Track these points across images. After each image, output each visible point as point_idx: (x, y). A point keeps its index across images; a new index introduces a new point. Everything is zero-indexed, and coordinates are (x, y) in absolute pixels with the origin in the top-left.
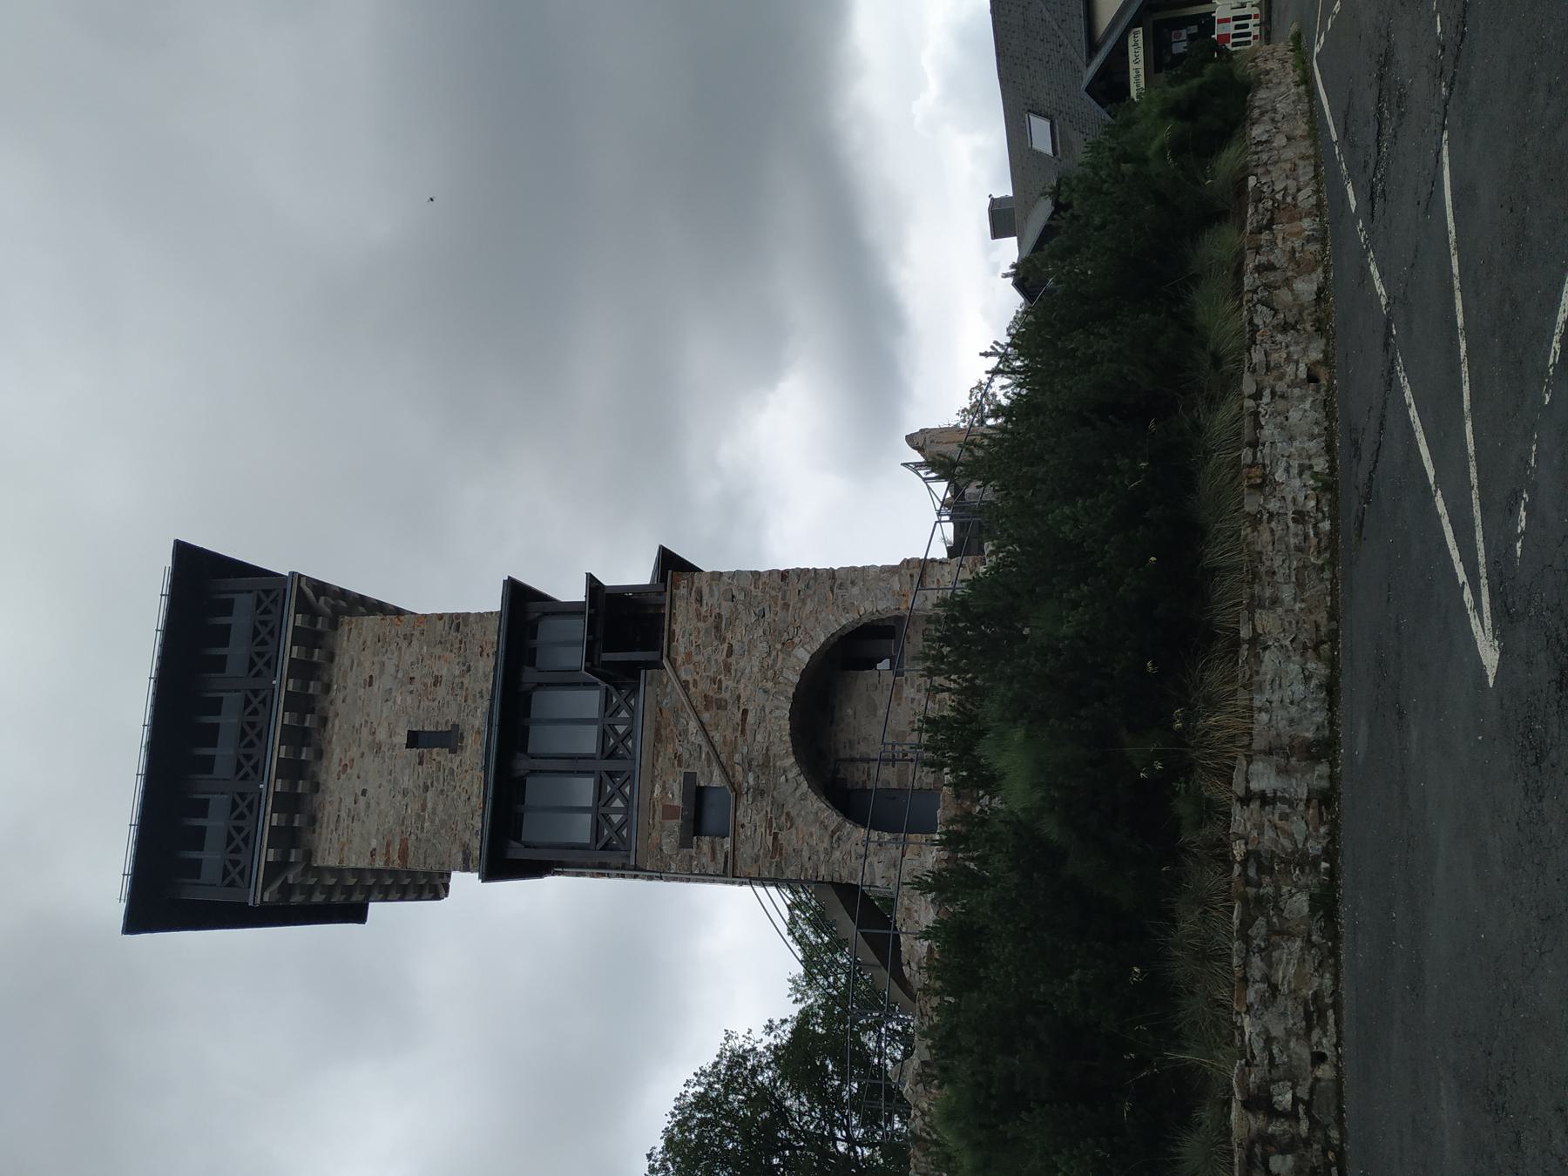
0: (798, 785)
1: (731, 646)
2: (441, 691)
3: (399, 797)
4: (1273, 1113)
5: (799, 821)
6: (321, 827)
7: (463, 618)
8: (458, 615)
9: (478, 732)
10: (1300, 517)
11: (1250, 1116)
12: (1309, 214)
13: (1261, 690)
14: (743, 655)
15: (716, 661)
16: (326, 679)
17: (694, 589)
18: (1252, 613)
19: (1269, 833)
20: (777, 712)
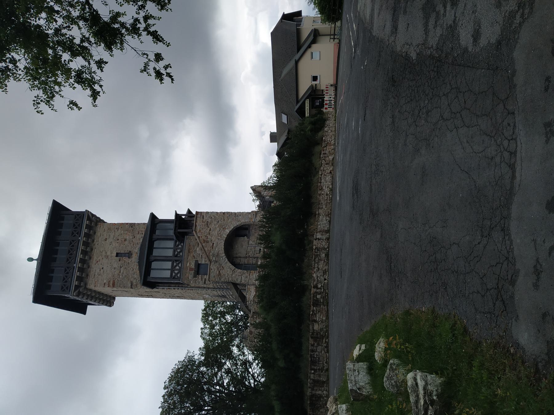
1: (210, 229)
2: (126, 242)
3: (113, 269)
4: (317, 288)
5: (225, 268)
6: (89, 277)
8: (132, 224)
9: (137, 253)
10: (327, 195)
11: (314, 289)
12: (333, 145)
13: (319, 222)
14: (213, 231)
15: (207, 232)
16: (93, 238)
18: (319, 210)
19: (319, 244)
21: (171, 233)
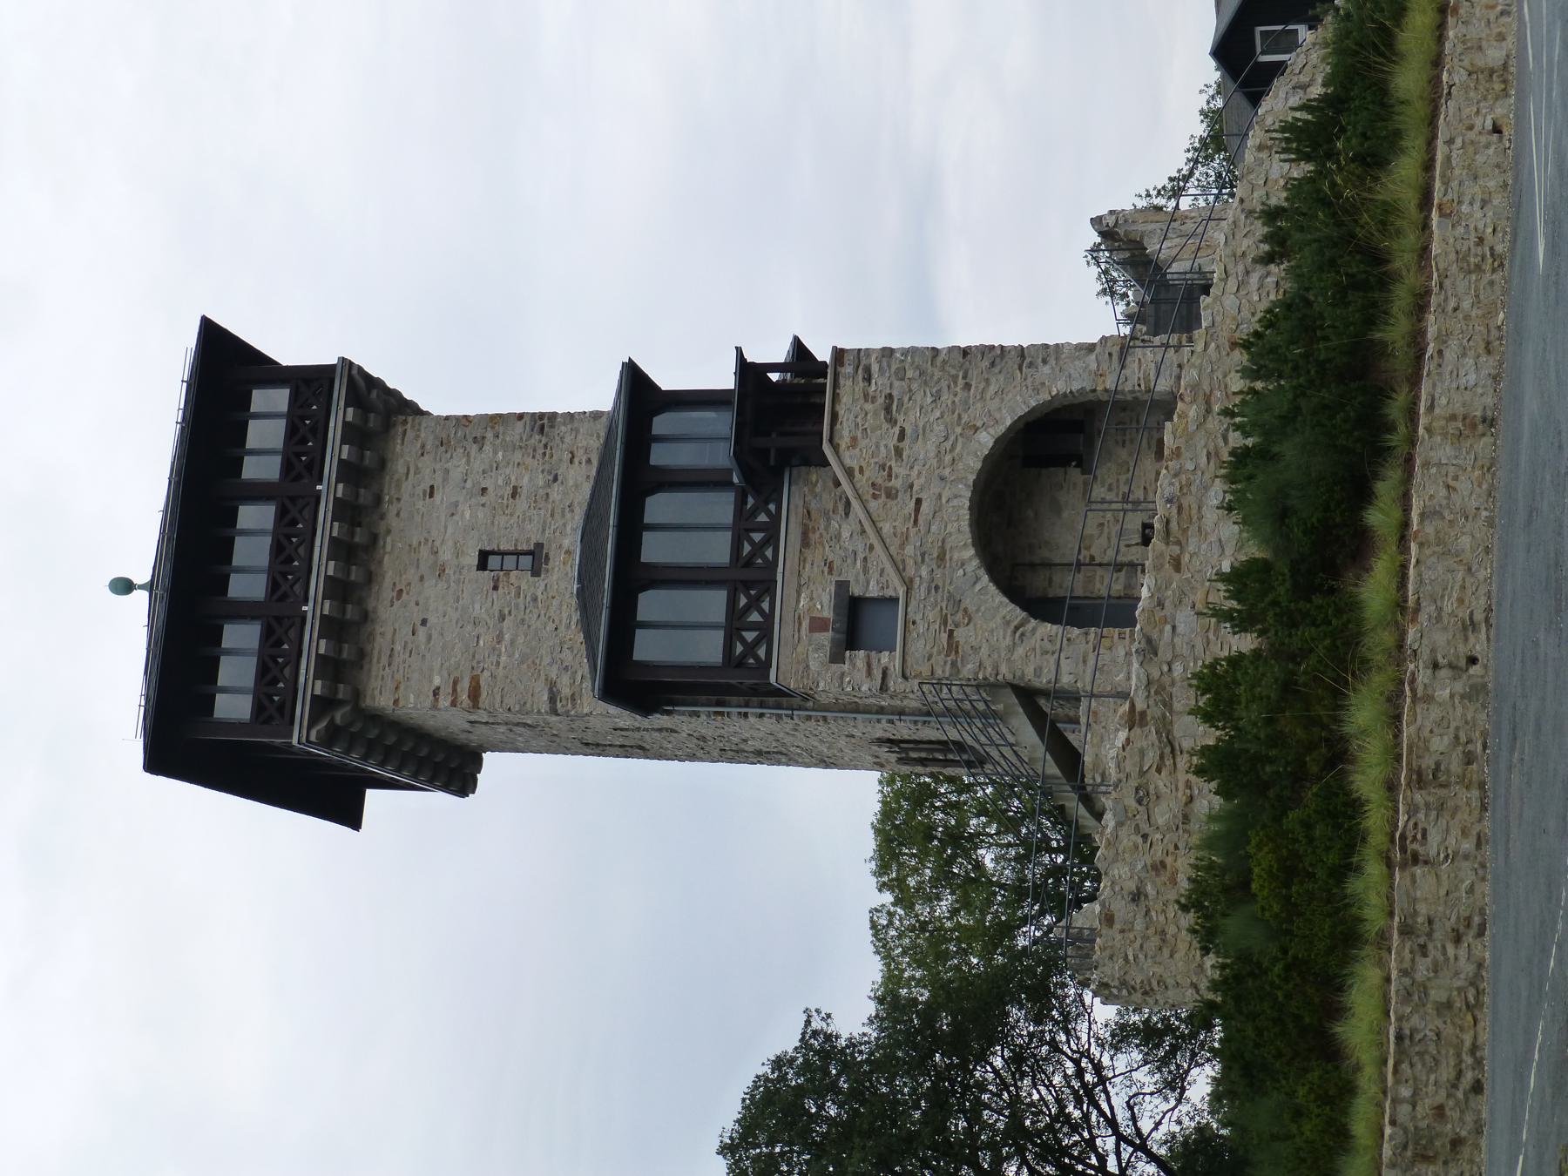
0: (978, 579)
2: (522, 504)
3: (469, 628)
7: (549, 419)
8: (542, 416)
17: (861, 368)
20: (955, 501)
21: (720, 456)
